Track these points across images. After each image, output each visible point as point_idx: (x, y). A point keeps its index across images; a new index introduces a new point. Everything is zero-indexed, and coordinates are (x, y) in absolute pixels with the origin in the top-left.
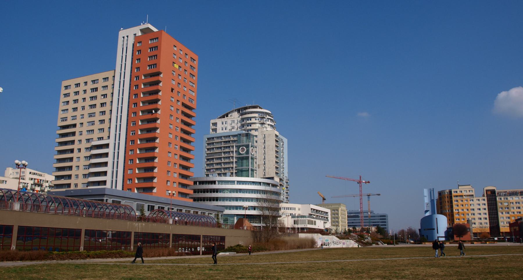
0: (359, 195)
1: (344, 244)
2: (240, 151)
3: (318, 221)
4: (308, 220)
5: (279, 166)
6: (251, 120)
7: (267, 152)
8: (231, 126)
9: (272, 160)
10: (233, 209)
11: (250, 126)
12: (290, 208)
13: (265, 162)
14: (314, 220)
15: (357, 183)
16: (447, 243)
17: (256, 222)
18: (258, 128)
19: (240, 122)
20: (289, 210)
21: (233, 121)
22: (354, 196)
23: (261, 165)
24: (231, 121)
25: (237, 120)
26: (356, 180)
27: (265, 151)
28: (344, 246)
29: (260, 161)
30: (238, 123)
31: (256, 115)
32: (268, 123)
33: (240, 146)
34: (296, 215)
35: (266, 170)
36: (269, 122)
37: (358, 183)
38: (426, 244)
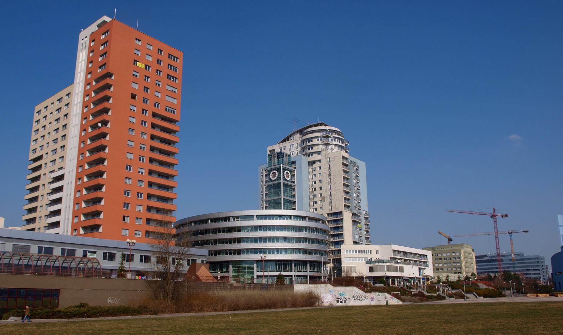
0: (494, 233)
1: (372, 299)
2: (271, 177)
3: (406, 267)
6: (312, 141)
8: (290, 151)
9: (340, 190)
10: (252, 253)
11: (312, 149)
12: (357, 251)
13: (331, 192)
14: (399, 265)
15: (490, 218)
16: (559, 295)
17: (285, 270)
18: (321, 150)
19: (300, 145)
20: (361, 253)
21: (293, 145)
22: (489, 235)
23: (326, 197)
24: (290, 145)
25: (297, 144)
26: (489, 214)
27: (330, 179)
28: (373, 303)
30: (298, 147)
31: (318, 134)
32: (334, 144)
33: (271, 170)
34: (373, 260)
35: (332, 203)
36: (336, 142)
37: (492, 217)
38: (529, 297)
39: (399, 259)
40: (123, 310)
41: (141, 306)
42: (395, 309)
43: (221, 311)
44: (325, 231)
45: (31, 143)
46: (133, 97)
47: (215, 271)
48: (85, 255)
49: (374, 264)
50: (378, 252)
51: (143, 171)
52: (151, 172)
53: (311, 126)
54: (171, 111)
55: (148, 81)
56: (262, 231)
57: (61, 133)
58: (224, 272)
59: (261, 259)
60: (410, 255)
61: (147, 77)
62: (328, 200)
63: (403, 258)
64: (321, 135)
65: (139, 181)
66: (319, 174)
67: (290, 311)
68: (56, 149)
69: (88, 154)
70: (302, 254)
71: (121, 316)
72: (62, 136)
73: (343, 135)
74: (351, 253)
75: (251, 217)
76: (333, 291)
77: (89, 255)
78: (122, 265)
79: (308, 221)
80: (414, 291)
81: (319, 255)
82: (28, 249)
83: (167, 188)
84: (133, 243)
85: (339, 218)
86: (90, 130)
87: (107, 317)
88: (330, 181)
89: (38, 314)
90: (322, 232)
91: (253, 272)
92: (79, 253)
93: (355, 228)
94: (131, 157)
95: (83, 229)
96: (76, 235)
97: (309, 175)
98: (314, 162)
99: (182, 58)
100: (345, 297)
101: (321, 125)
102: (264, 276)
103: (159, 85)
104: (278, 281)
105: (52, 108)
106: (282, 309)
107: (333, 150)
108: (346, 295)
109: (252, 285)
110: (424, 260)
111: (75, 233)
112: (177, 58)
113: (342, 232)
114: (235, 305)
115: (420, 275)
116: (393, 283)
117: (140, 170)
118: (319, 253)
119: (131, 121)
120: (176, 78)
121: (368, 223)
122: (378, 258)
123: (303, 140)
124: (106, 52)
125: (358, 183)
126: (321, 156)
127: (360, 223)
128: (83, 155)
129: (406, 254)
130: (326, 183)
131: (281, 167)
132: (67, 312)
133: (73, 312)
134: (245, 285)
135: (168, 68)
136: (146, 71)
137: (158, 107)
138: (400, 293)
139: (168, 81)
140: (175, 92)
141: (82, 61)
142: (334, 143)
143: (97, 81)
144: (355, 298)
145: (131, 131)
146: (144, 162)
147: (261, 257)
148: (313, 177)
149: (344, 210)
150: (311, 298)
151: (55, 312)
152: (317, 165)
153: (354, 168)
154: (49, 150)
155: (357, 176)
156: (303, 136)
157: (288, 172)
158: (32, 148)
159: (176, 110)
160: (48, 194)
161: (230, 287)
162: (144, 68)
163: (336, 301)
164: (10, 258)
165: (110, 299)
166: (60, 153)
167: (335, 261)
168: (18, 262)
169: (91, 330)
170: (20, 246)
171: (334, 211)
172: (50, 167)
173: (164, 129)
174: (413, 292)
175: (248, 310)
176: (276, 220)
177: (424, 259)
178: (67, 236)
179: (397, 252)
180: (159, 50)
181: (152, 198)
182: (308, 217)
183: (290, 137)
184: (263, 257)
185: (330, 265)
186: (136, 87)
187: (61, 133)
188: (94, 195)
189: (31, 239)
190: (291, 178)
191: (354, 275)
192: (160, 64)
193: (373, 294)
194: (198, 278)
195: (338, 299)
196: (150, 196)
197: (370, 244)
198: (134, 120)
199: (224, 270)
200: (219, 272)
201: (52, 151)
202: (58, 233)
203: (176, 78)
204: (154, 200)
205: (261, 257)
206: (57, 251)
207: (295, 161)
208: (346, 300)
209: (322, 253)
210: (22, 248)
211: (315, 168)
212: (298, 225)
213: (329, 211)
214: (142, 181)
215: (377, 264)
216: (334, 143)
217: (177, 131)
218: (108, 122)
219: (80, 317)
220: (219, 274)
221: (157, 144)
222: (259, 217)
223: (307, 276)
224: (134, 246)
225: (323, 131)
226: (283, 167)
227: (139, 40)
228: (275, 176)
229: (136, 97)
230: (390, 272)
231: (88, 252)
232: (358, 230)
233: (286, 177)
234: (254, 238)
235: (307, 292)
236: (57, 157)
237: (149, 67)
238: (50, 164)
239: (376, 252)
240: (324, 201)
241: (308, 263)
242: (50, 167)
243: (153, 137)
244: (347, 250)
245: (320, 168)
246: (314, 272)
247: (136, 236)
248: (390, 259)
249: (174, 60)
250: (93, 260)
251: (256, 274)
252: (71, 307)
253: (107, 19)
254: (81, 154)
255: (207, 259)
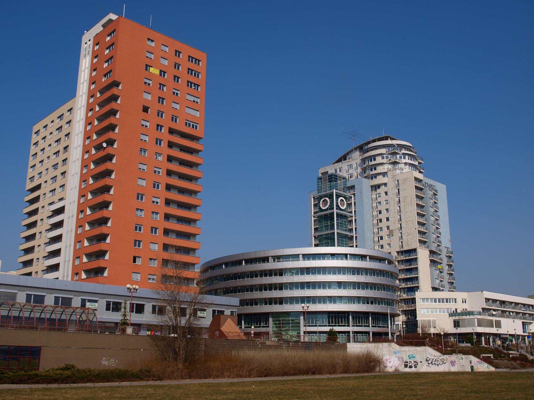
1: (453, 363)
2: (321, 206)
3: (505, 322)
4: (479, 320)
5: (426, 230)
6: (375, 160)
7: (403, 208)
8: (348, 173)
11: (375, 169)
12: (437, 299)
13: (401, 224)
14: (494, 319)
18: (387, 171)
19: (360, 165)
20: (443, 302)
21: (351, 166)
23: (395, 230)
24: (348, 166)
25: (356, 163)
27: (400, 207)
28: (454, 369)
29: (394, 224)
30: (357, 167)
31: (383, 151)
32: (404, 162)
33: (321, 197)
34: (459, 311)
35: (403, 238)
36: (407, 160)
39: (494, 310)
40: (117, 374)
41: (143, 370)
42: (481, 378)
43: (247, 376)
44: (392, 274)
45: (28, 170)
46: (146, 109)
47: (260, 324)
48: (83, 305)
49: (460, 317)
50: (465, 301)
51: (159, 200)
52: (168, 202)
53: (374, 141)
54: (193, 125)
55: (163, 90)
56: (309, 274)
57: (62, 156)
58: (263, 327)
59: (302, 310)
60: (509, 305)
61: (162, 85)
62: (397, 234)
63: (499, 309)
64: (387, 152)
65: (153, 212)
66: (385, 201)
67: (338, 379)
68: (56, 176)
69: (91, 181)
70: (363, 304)
71: (115, 382)
72: (63, 161)
73: (415, 150)
74: (430, 303)
75: (295, 257)
76: (399, 351)
77: (88, 305)
78: (125, 318)
79: (369, 261)
80: (513, 353)
81: (385, 305)
82: (13, 296)
83: (189, 221)
84: (134, 289)
85: (413, 257)
86: (93, 152)
87: (97, 383)
88: (400, 210)
89: (9, 378)
90: (388, 275)
91: (299, 326)
92: (76, 302)
93: (434, 269)
94: (143, 183)
95: (84, 273)
96: (77, 280)
97: (372, 203)
98: (378, 186)
99: (206, 60)
100: (415, 360)
101: (386, 138)
102: (307, 332)
103: (177, 94)
104: (329, 339)
105: (52, 127)
106: (330, 375)
107: (403, 169)
108: (416, 357)
109: (290, 343)
110: (529, 312)
111: (76, 278)
112: (199, 61)
113: (416, 276)
114: (266, 370)
115: (524, 332)
116: (487, 342)
117: (154, 199)
118: (385, 302)
119: (143, 140)
120: (198, 86)
121: (451, 264)
122: (466, 309)
123: (363, 159)
124: (112, 57)
125: (436, 211)
126: (387, 178)
127: (441, 263)
128: (86, 182)
129: (504, 304)
130: (395, 212)
131: (333, 192)
132: (45, 376)
133: (53, 377)
134: (281, 343)
135: (188, 73)
136: (160, 77)
137: (176, 121)
138: (492, 355)
139: (189, 90)
140: (197, 102)
141: (85, 69)
142: (404, 161)
143: (102, 92)
144: (430, 362)
145: (143, 151)
146: (160, 190)
147: (303, 307)
148: (377, 206)
149: (418, 247)
150: (370, 362)
151: (30, 375)
152: (383, 189)
153: (431, 193)
154: (48, 178)
155: (435, 203)
156: (363, 154)
157: (343, 199)
158: (29, 176)
159: (198, 124)
160: (46, 230)
161: (262, 346)
162: (158, 74)
163: (403, 366)
164: (20, 309)
165: (104, 359)
166: (60, 181)
167: (408, 313)
168: (7, 313)
169: (231, 387)
170: (4, 294)
171: (405, 248)
172: (49, 197)
173: (184, 149)
174: (512, 354)
175: (284, 376)
176: (328, 260)
177: (530, 310)
178: (67, 281)
179: (491, 301)
180: (176, 51)
181: (170, 234)
182: (369, 256)
183: (347, 156)
184: (306, 308)
185: (401, 319)
186: (149, 97)
187: (62, 156)
188: (98, 231)
189: (54, 288)
190: (347, 206)
191: (432, 331)
192: (178, 69)
193: (453, 357)
194: (222, 334)
195: (405, 362)
196: (167, 232)
197: (455, 290)
198: (147, 138)
199: (262, 324)
200: (253, 327)
201: (51, 179)
202: (58, 278)
203: (198, 86)
204: (172, 237)
205: (303, 307)
206: (49, 300)
207: (354, 185)
208: (417, 364)
209: (389, 302)
210: (6, 296)
211: (380, 193)
212: (357, 267)
213: (399, 248)
214: (157, 213)
215: (464, 317)
216: (404, 161)
217: (201, 151)
218: (115, 141)
219: (62, 382)
220: (253, 329)
221: (175, 167)
222: (307, 257)
223: (370, 332)
224: (136, 292)
225: (390, 146)
226: (336, 192)
227: (152, 41)
228: (326, 205)
229: (149, 110)
230: (483, 328)
231: (87, 301)
232: (438, 272)
233: (340, 206)
234: (299, 284)
235: (356, 354)
236: (57, 185)
237: (165, 72)
238: (49, 195)
239: (463, 301)
240: (393, 236)
241: (370, 315)
242: (49, 197)
243: (170, 159)
244: (423, 299)
245: (386, 193)
246: (378, 327)
247: (149, 281)
248: (481, 311)
249: (195, 63)
250: (88, 310)
251: (303, 329)
252: (53, 369)
253: (113, 17)
254: (84, 181)
255: (237, 310)
